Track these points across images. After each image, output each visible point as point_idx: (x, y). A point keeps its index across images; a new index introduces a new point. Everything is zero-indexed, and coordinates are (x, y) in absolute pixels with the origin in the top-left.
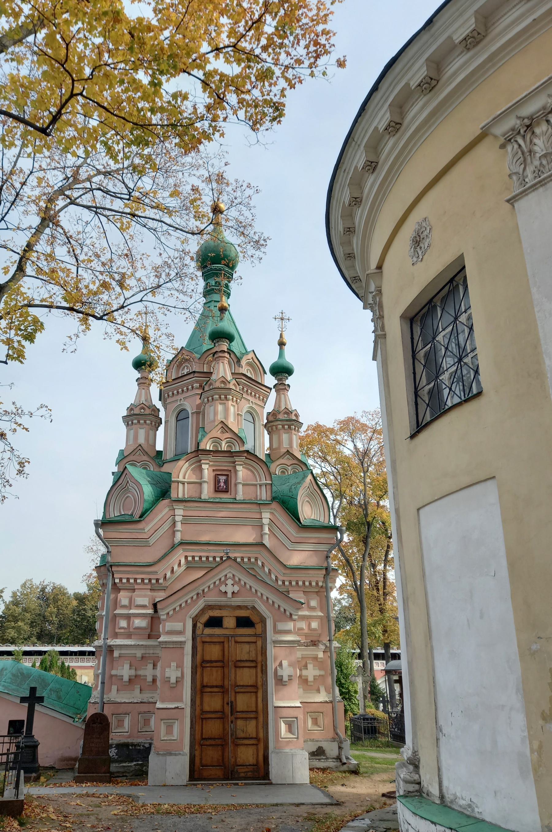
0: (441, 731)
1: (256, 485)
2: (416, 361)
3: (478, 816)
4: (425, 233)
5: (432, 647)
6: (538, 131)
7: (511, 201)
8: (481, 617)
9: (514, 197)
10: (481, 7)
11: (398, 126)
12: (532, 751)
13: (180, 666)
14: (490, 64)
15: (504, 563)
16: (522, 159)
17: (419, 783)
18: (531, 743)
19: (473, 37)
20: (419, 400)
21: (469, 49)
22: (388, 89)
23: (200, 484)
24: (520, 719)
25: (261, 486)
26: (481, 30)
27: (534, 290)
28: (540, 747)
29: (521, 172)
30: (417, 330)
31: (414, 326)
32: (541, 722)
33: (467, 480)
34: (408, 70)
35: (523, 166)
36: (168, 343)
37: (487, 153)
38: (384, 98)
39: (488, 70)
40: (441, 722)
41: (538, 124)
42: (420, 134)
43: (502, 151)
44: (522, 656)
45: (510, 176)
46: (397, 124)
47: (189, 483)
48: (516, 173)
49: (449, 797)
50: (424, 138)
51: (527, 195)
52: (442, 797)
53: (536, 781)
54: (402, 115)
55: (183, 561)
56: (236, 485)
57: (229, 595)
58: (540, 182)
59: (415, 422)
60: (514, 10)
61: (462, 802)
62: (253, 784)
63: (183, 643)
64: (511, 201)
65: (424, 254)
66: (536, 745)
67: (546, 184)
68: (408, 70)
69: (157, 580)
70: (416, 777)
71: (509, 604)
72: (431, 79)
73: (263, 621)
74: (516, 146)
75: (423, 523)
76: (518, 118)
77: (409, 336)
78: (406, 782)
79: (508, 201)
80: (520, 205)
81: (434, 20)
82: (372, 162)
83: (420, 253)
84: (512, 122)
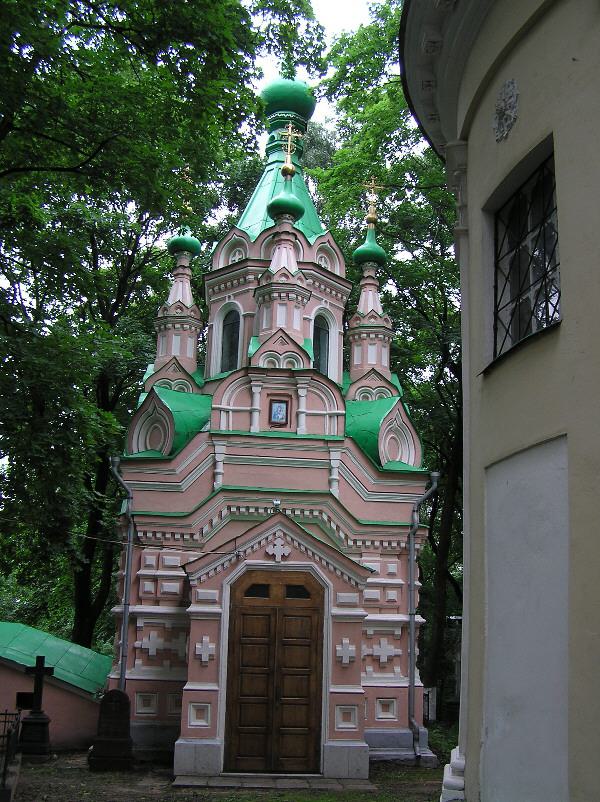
1: (324, 415)
13: (217, 640)
23: (251, 412)
25: (331, 416)
47: (234, 411)
55: (225, 512)
56: (298, 414)
57: (278, 558)
63: (219, 615)
69: (192, 535)
73: (321, 589)
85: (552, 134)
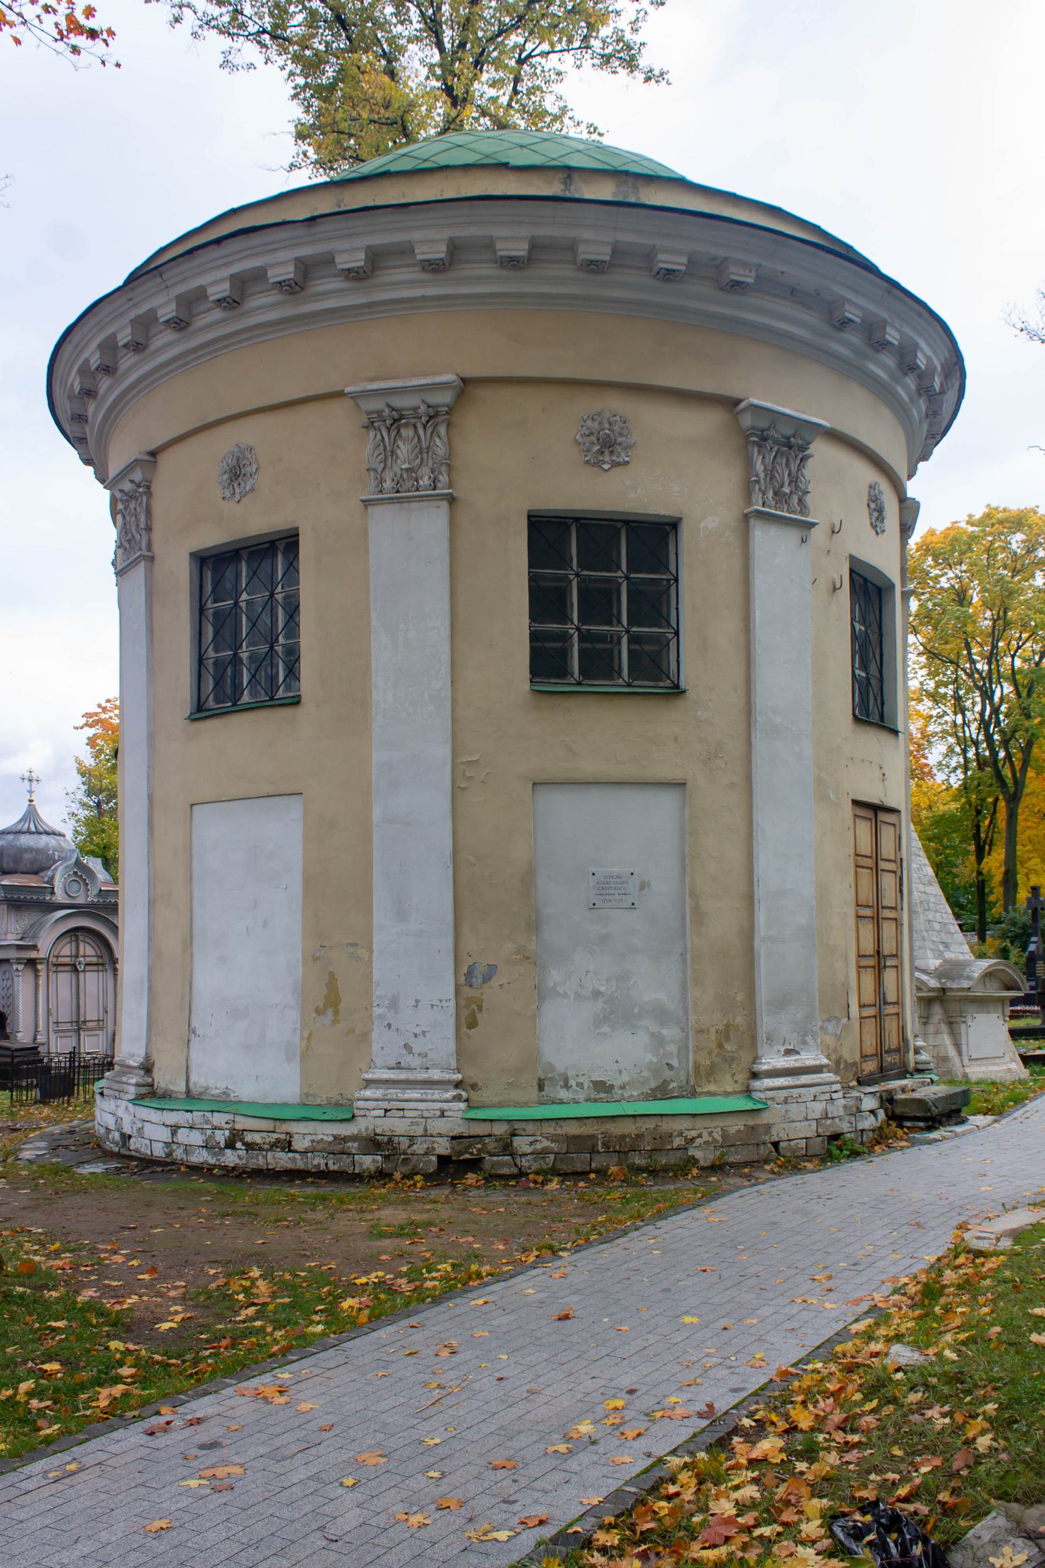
0: (194, 1032)
2: (203, 618)
3: (233, 1099)
4: (249, 469)
5: (192, 954)
7: (366, 503)
8: (264, 926)
12: (302, 1039)
15: (299, 878)
16: (382, 456)
17: (152, 1085)
18: (302, 1031)
19: (357, 273)
20: (203, 670)
24: (293, 1015)
27: (373, 615)
28: (310, 1035)
29: (380, 471)
30: (209, 575)
31: (205, 568)
32: (314, 1015)
33: (269, 789)
34: (268, 251)
35: (382, 465)
36: (124, 336)
37: (341, 420)
38: (226, 260)
40: (195, 1024)
41: (406, 425)
43: (364, 430)
44: (305, 963)
45: (368, 470)
46: (234, 301)
48: (375, 470)
49: (195, 1091)
50: (266, 338)
52: (188, 1092)
53: (301, 1061)
58: (398, 498)
59: (196, 698)
60: (406, 270)
61: (214, 1092)
64: (366, 503)
65: (243, 495)
66: (306, 1034)
68: (268, 251)
70: (150, 1080)
71: (298, 916)
74: (379, 437)
75: (195, 820)
77: (198, 582)
78: (138, 1085)
79: (363, 501)
80: (375, 511)
81: (319, 220)
83: (237, 491)
84: (378, 404)
85: (200, 711)
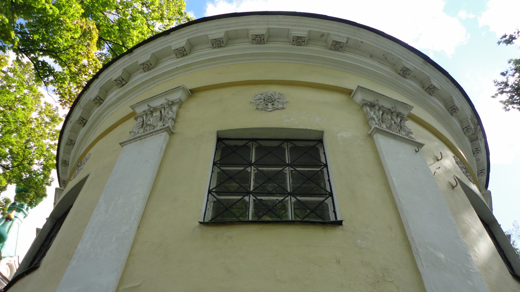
6: (154, 114)
7: (122, 144)
9: (124, 143)
10: (158, 51)
11: (101, 101)
14: (152, 82)
21: (145, 71)
22: (102, 79)
26: (153, 64)
39: (151, 85)
42: (110, 109)
45: (130, 132)
46: (101, 99)
51: (131, 143)
54: (106, 96)
62: (329, 180)
64: (122, 144)
67: (142, 139)
72: (123, 80)
74: (142, 120)
76: (149, 106)
80: (126, 147)
82: (84, 119)
